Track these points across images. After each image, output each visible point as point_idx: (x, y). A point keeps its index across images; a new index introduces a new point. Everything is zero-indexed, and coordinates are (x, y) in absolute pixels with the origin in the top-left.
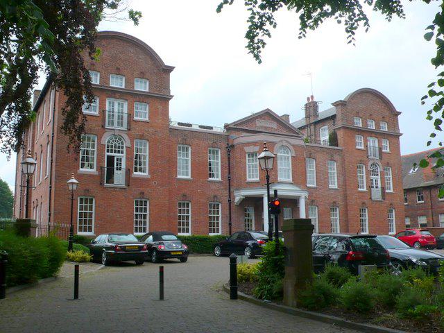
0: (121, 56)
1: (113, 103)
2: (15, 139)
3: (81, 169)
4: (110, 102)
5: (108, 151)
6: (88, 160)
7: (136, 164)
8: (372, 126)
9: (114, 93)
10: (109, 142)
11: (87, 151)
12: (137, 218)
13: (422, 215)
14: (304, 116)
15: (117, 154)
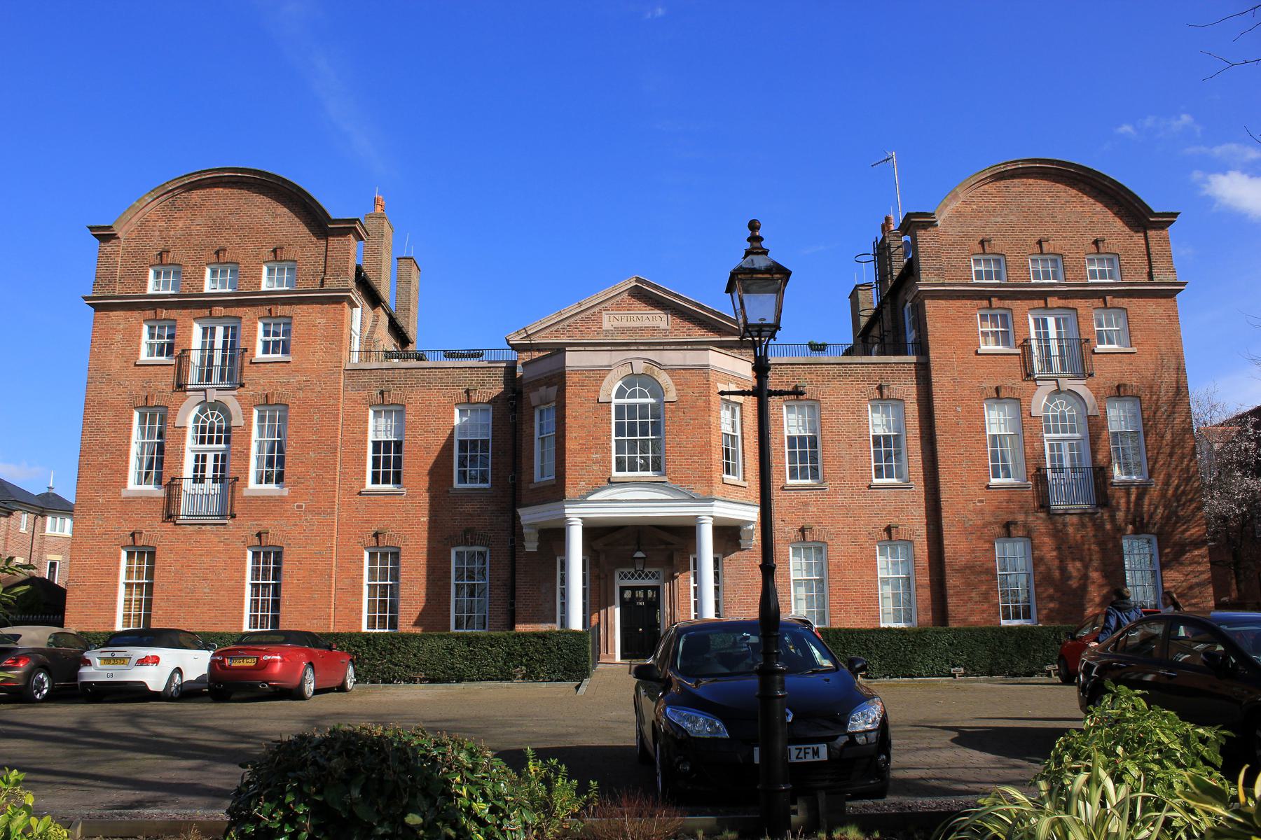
1: (1045, 321)
4: (1036, 321)
15: (215, 446)
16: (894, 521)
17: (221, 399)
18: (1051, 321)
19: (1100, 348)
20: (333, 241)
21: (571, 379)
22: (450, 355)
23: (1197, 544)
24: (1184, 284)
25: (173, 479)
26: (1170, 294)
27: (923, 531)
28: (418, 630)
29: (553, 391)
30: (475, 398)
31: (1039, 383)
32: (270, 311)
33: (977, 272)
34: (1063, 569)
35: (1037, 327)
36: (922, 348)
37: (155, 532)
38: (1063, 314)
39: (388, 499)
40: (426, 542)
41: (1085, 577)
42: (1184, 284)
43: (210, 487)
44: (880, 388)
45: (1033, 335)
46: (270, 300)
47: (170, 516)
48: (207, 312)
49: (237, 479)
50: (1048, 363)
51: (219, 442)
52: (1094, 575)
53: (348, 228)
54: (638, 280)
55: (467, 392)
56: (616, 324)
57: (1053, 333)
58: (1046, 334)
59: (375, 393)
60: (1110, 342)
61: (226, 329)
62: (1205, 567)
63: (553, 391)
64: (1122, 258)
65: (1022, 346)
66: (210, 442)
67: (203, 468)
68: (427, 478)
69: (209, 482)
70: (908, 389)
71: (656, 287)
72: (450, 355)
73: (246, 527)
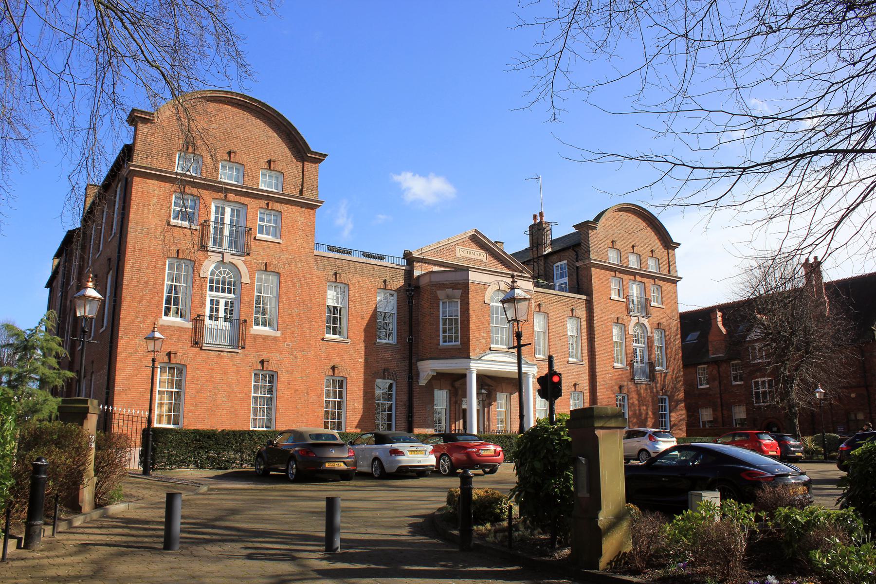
0: (239, 131)
1: (223, 209)
2: (804, 280)
3: (164, 318)
4: (217, 207)
5: (211, 289)
6: (176, 303)
7: (257, 312)
8: (633, 263)
9: (222, 190)
10: (212, 273)
11: (175, 286)
12: (256, 403)
13: (705, 406)
14: (526, 244)
15: (226, 295)
16: (577, 381)
17: (234, 261)
18: (228, 210)
19: (259, 236)
20: (308, 165)
21: (472, 288)
22: (366, 255)
23: (681, 401)
24: (322, 202)
25: (199, 316)
26: (313, 207)
27: (587, 387)
28: (358, 431)
29: (458, 293)
30: (388, 287)
31: (210, 253)
32: (268, 204)
33: (613, 258)
34: (640, 410)
35: (217, 213)
36: (589, 293)
37: (186, 354)
38: (236, 207)
39: (340, 345)
40: (362, 375)
41: (647, 414)
42: (322, 202)
43: (221, 324)
44: (572, 310)
45: (213, 219)
46: (268, 198)
47: (196, 343)
48: (222, 196)
49: (245, 321)
50: (218, 242)
51: (229, 292)
52: (650, 413)
53: (318, 159)
54: (476, 231)
55: (385, 281)
56: (463, 254)
57: (227, 220)
58: (223, 219)
59: (332, 273)
60: (268, 234)
61: (232, 210)
62: (684, 412)
63: (458, 293)
64: (246, 168)
65: (202, 225)
66: (223, 291)
67: (217, 310)
68: (363, 334)
69: (221, 320)
70: (582, 313)
71: (484, 237)
72: (366, 255)
73: (249, 357)
